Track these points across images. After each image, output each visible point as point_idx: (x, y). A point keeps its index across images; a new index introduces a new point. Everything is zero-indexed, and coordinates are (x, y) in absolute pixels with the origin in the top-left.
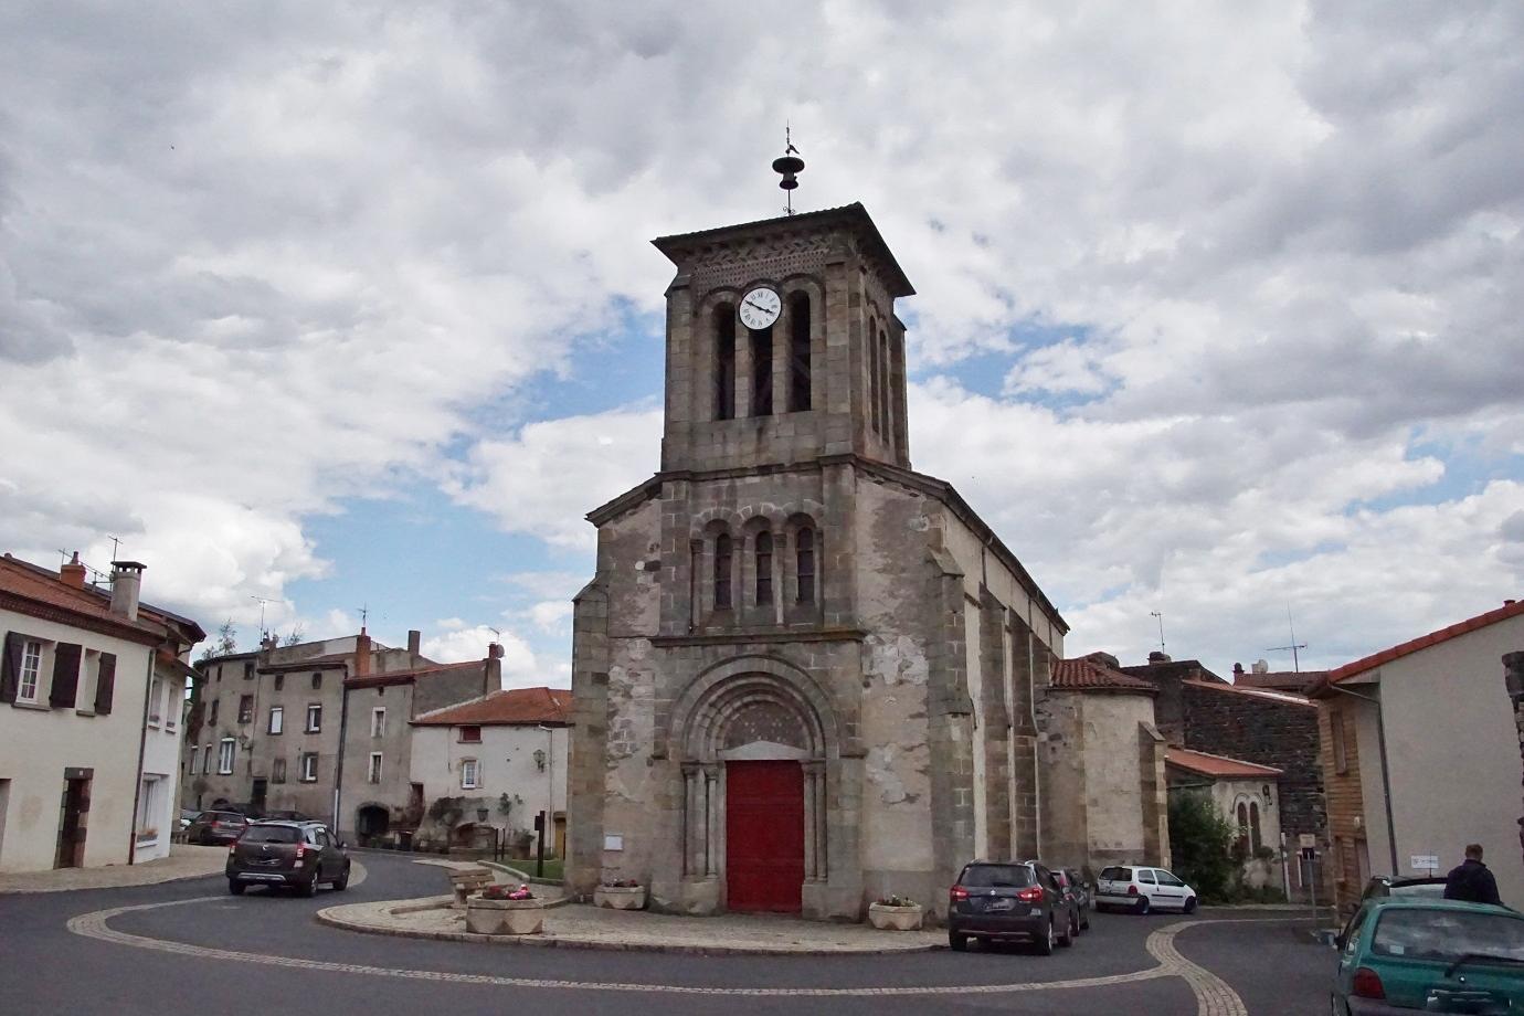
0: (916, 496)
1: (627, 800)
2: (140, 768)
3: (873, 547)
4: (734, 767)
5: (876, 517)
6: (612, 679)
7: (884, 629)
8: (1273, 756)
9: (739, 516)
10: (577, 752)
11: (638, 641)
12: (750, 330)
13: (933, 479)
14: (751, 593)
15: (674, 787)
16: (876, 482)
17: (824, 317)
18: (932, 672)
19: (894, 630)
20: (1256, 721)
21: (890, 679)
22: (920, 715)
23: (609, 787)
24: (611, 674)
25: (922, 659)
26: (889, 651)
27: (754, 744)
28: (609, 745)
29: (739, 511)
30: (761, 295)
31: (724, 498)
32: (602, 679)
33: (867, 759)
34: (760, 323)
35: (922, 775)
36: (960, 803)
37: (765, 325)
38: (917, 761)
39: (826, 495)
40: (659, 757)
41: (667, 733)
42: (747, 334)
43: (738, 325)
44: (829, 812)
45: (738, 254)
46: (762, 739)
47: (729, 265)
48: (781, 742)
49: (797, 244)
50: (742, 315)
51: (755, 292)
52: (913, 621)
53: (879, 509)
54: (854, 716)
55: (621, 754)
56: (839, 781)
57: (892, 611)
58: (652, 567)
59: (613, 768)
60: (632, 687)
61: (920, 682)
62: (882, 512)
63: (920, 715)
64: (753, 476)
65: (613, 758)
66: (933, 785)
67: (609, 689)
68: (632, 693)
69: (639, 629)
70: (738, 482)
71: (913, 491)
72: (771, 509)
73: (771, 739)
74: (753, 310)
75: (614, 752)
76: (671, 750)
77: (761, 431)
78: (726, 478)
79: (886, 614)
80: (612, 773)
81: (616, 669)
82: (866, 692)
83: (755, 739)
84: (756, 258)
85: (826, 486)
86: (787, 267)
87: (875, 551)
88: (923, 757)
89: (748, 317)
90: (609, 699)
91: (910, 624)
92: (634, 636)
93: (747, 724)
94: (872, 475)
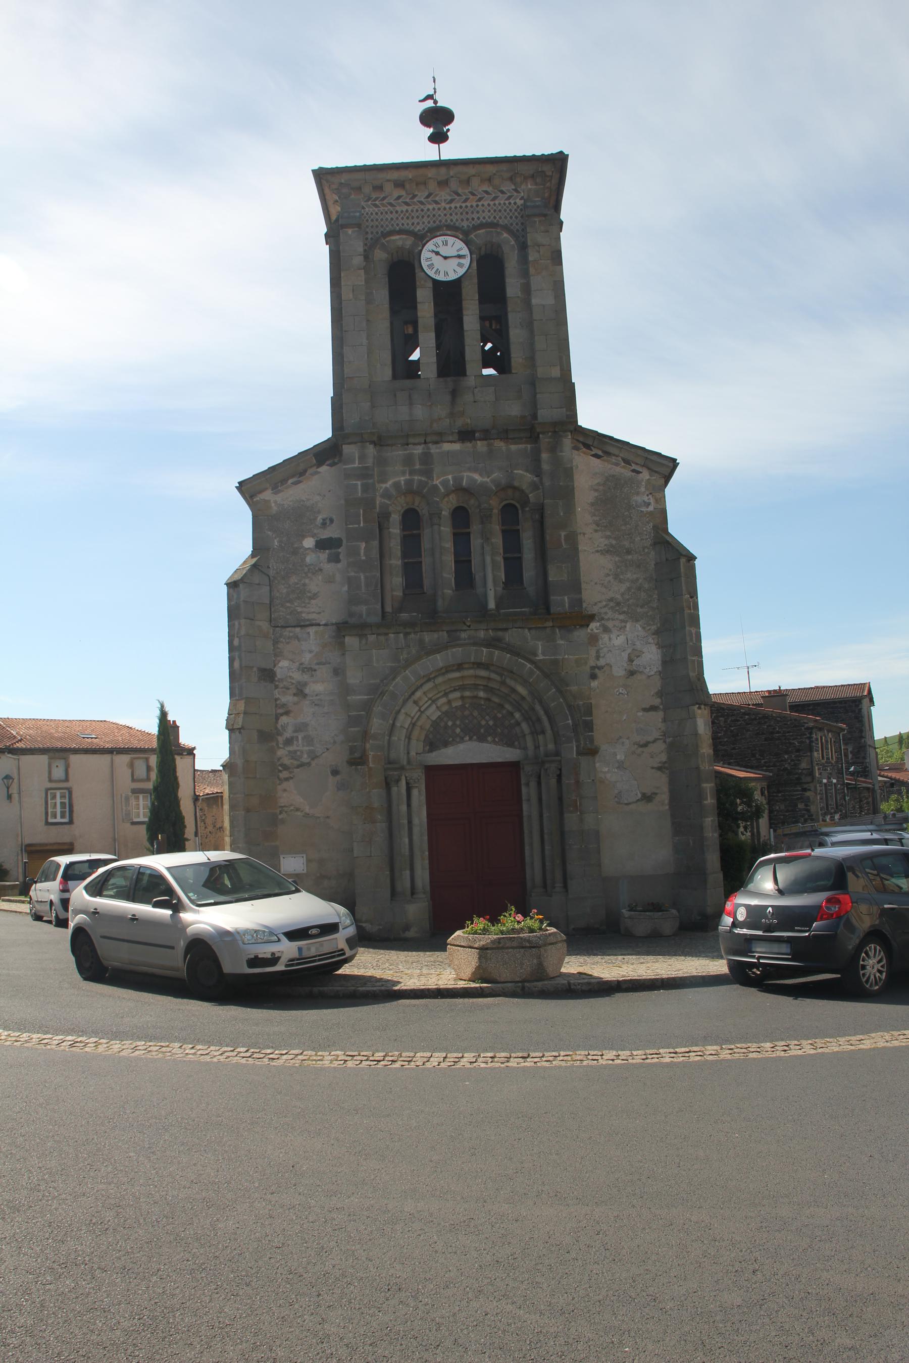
0: (638, 472)
1: (307, 815)
2: (76, 751)
3: (594, 527)
4: (432, 772)
5: (596, 494)
6: (279, 676)
7: (610, 614)
8: (763, 761)
9: (435, 487)
10: (723, 709)
11: (312, 630)
12: (435, 282)
13: (659, 455)
14: (449, 574)
15: (377, 796)
16: (593, 456)
17: (525, 274)
18: (664, 663)
19: (622, 617)
20: (749, 730)
21: (619, 671)
22: (653, 708)
23: (282, 802)
24: (278, 671)
25: (654, 648)
26: (618, 641)
27: (461, 746)
28: (280, 753)
29: (437, 482)
30: (446, 243)
31: (417, 467)
32: (268, 675)
33: (597, 758)
34: (446, 274)
35: (659, 773)
36: (707, 799)
37: (452, 277)
38: (652, 757)
39: (545, 467)
40: (357, 760)
41: (365, 735)
42: (430, 284)
43: (419, 275)
44: (566, 815)
45: (414, 196)
46: (471, 739)
47: (405, 208)
48: (494, 742)
49: (486, 192)
50: (424, 264)
51: (439, 240)
52: (642, 607)
53: (598, 484)
54: (589, 711)
55: (296, 763)
56: (577, 782)
57: (619, 597)
58: (322, 545)
59: (287, 779)
60: (306, 684)
61: (652, 673)
62: (601, 488)
63: (653, 708)
64: (451, 442)
65: (286, 768)
66: (672, 782)
67: (276, 687)
68: (307, 691)
69: (311, 616)
70: (434, 449)
71: (634, 467)
72: (476, 480)
73: (482, 739)
74: (437, 260)
75: (287, 761)
76: (371, 754)
77: (454, 394)
78: (420, 444)
79: (611, 600)
80: (285, 785)
81: (284, 663)
82: (594, 684)
83: (462, 740)
84: (436, 203)
85: (545, 456)
86: (475, 216)
87: (596, 531)
88: (659, 752)
89: (431, 266)
90: (276, 700)
91: (639, 610)
92: (304, 625)
93: (450, 723)
94: (588, 447)
